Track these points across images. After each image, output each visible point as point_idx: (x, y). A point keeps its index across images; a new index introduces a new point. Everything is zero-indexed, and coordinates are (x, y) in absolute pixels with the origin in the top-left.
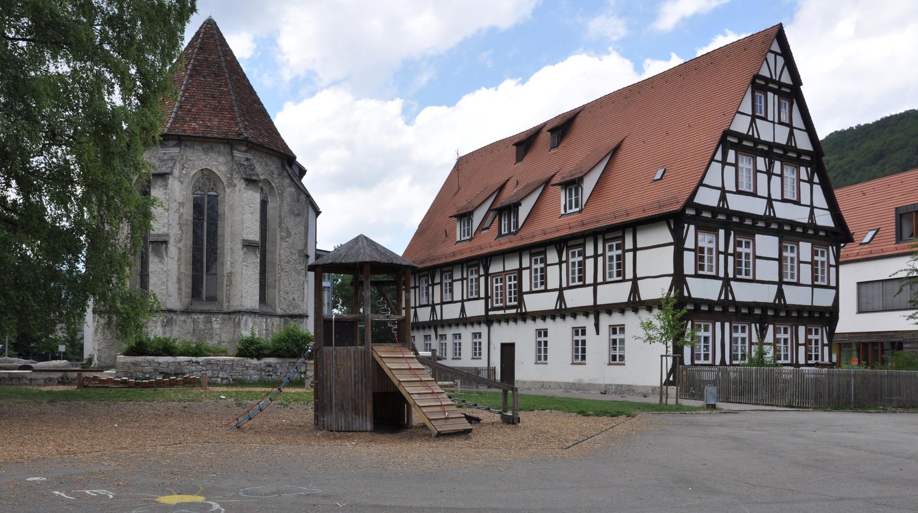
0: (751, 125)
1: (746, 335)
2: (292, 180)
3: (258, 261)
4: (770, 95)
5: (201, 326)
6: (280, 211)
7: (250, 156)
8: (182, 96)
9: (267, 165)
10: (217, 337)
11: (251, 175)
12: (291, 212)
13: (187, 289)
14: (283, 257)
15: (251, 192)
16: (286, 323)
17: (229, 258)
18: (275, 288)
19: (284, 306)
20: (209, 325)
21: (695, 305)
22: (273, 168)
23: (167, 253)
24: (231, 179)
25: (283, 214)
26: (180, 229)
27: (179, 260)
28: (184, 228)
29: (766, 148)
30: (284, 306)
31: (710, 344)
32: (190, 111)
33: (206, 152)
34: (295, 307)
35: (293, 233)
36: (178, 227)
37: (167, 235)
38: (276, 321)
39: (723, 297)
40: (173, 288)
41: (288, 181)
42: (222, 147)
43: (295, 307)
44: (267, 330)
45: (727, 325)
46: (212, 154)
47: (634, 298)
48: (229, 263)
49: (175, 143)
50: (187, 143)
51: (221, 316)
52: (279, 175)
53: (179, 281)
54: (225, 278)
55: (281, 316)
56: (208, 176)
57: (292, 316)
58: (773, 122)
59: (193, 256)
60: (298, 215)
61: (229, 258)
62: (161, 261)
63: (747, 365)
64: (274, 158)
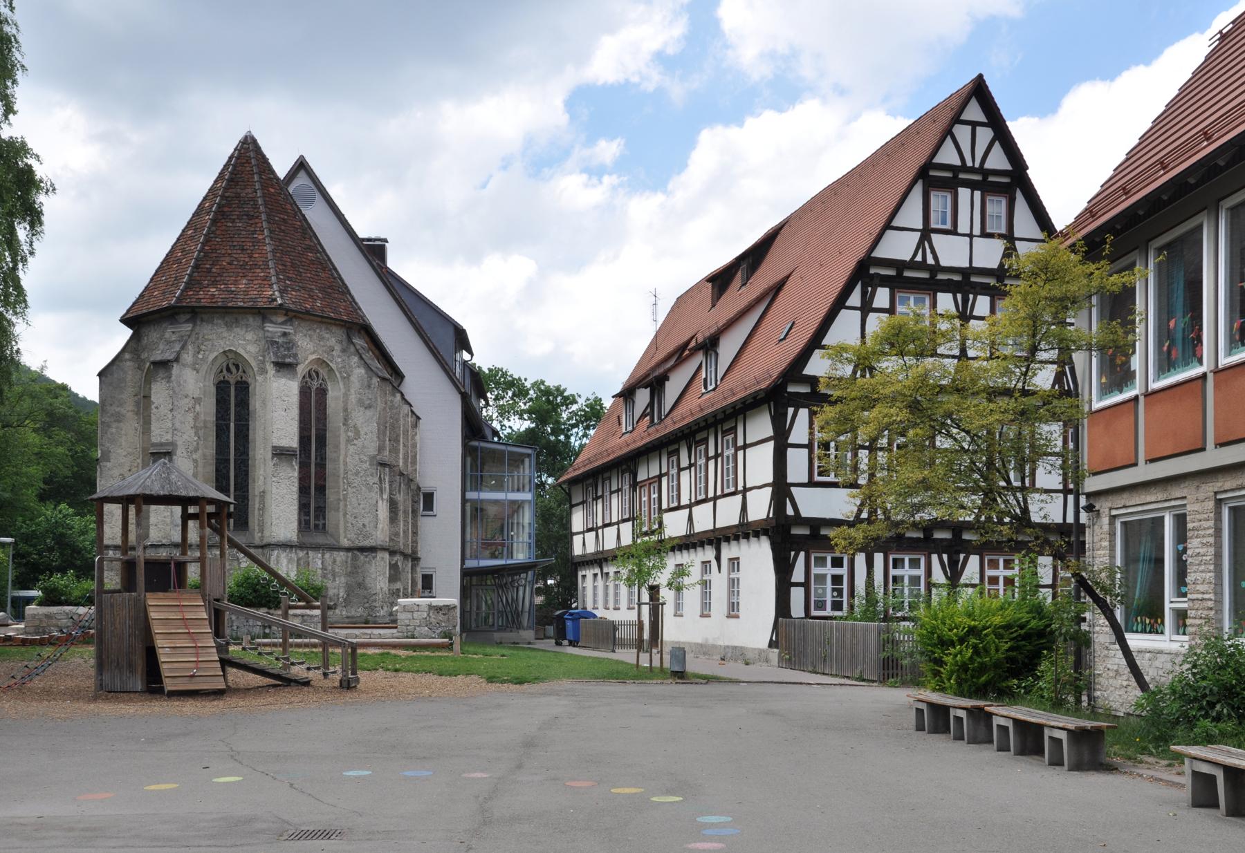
0: (920, 244)
1: (921, 572)
2: (361, 358)
3: (296, 474)
4: (964, 193)
7: (289, 329)
8: (200, 252)
9: (321, 338)
11: (284, 356)
12: (361, 402)
14: (350, 467)
15: (283, 380)
16: (355, 558)
18: (337, 510)
19: (352, 535)
21: (812, 528)
22: (332, 341)
24: (263, 362)
25: (350, 407)
26: (196, 434)
28: (201, 433)
29: (957, 278)
30: (352, 535)
31: (845, 586)
32: (209, 271)
33: (229, 326)
34: (366, 537)
35: (362, 433)
36: (192, 432)
37: (173, 444)
38: (341, 556)
41: (356, 359)
42: (251, 319)
43: (366, 537)
44: (324, 568)
45: (879, 558)
46: (237, 330)
49: (188, 316)
52: (344, 351)
54: (257, 499)
55: (348, 549)
56: (233, 362)
57: (362, 549)
58: (971, 236)
59: (217, 470)
60: (369, 407)
63: (846, 619)
64: (334, 329)
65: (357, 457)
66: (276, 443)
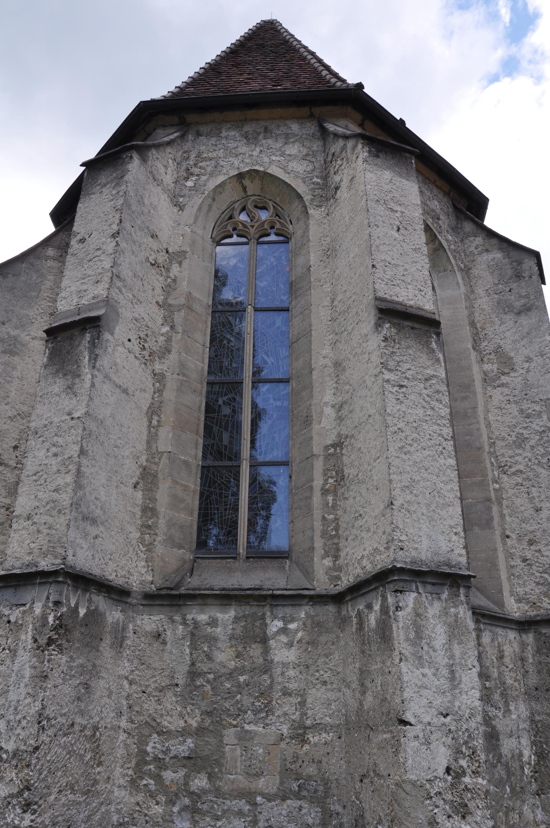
5: (224, 656)
6: (470, 308)
10: (288, 707)
12: (504, 307)
13: (179, 498)
17: (328, 397)
19: (530, 588)
20: (255, 650)
23: (94, 358)
27: (154, 411)
28: (179, 318)
35: (518, 359)
40: (116, 497)
48: (329, 411)
50: (202, 129)
51: (303, 612)
53: (147, 479)
54: (319, 465)
55: (523, 625)
59: (209, 409)
61: (328, 397)
65: (514, 409)
66: (385, 291)
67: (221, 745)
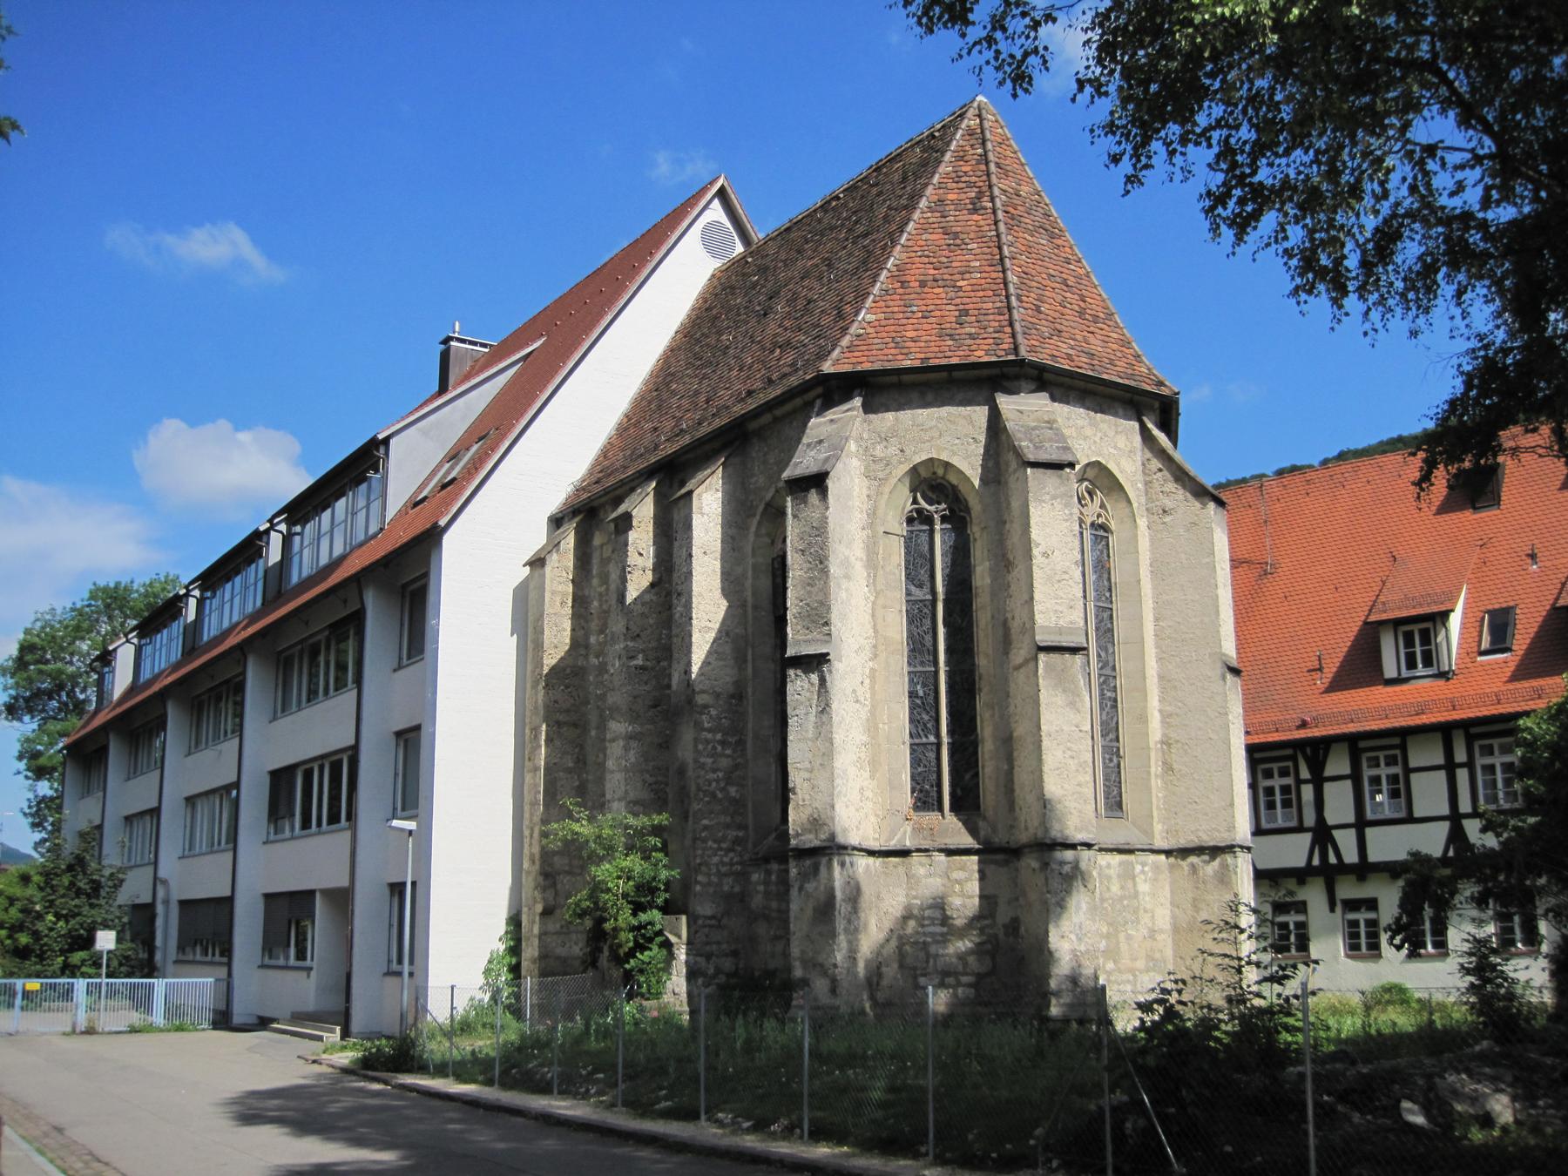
10: (1145, 919)
20: (1130, 884)
39: (1316, 862)
47: (1324, 856)
62: (1072, 704)
67: (1118, 943)
